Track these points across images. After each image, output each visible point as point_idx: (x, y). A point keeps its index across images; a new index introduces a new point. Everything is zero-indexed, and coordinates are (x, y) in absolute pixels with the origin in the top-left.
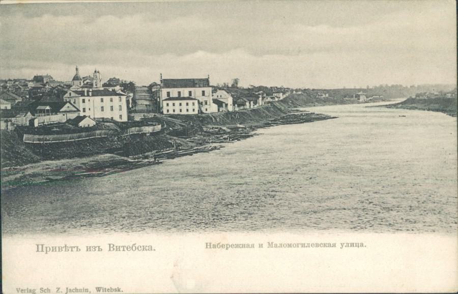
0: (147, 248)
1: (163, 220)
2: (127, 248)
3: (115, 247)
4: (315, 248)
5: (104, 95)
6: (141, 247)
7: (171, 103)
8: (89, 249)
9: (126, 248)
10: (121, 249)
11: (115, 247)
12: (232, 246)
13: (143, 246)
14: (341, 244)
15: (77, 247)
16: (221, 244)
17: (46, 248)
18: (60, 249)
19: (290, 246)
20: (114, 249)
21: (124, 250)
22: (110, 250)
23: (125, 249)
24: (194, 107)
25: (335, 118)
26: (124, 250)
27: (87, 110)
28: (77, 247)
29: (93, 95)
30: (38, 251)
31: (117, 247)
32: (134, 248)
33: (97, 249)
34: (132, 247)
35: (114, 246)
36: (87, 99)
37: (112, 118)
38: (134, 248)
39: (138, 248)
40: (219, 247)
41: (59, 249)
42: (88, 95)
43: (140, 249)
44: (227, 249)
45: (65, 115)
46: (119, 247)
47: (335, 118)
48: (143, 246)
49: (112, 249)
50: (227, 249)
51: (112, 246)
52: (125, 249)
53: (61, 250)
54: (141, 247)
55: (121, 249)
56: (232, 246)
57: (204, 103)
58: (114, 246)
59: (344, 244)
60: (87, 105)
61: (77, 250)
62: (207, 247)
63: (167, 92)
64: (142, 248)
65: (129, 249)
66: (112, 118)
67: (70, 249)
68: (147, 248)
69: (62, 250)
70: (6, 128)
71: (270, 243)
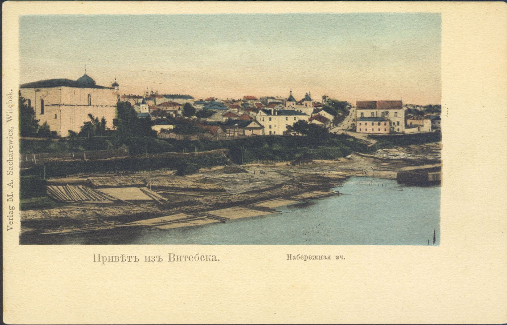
0: (211, 258)
3: (176, 257)
5: (319, 112)
6: (204, 257)
7: (363, 123)
8: (148, 259)
11: (176, 257)
12: (310, 258)
15: (342, 259)
16: (300, 256)
17: (103, 257)
18: (117, 259)
19: (315, 258)
23: (187, 259)
24: (385, 127)
27: (273, 127)
28: (342, 259)
29: (278, 114)
30: (146, 261)
32: (197, 259)
33: (133, 260)
35: (174, 255)
36: (273, 117)
38: (197, 259)
39: (309, 258)
40: (298, 258)
41: (322, 258)
42: (274, 114)
43: (203, 259)
44: (305, 260)
45: (252, 131)
49: (172, 259)
50: (305, 260)
52: (187, 259)
53: (117, 260)
54: (204, 257)
55: (183, 259)
56: (310, 258)
57: (396, 124)
58: (174, 255)
61: (159, 261)
62: (342, 256)
63: (270, 125)
64: (205, 257)
65: (191, 259)
67: (128, 260)
68: (211, 258)
69: (119, 260)
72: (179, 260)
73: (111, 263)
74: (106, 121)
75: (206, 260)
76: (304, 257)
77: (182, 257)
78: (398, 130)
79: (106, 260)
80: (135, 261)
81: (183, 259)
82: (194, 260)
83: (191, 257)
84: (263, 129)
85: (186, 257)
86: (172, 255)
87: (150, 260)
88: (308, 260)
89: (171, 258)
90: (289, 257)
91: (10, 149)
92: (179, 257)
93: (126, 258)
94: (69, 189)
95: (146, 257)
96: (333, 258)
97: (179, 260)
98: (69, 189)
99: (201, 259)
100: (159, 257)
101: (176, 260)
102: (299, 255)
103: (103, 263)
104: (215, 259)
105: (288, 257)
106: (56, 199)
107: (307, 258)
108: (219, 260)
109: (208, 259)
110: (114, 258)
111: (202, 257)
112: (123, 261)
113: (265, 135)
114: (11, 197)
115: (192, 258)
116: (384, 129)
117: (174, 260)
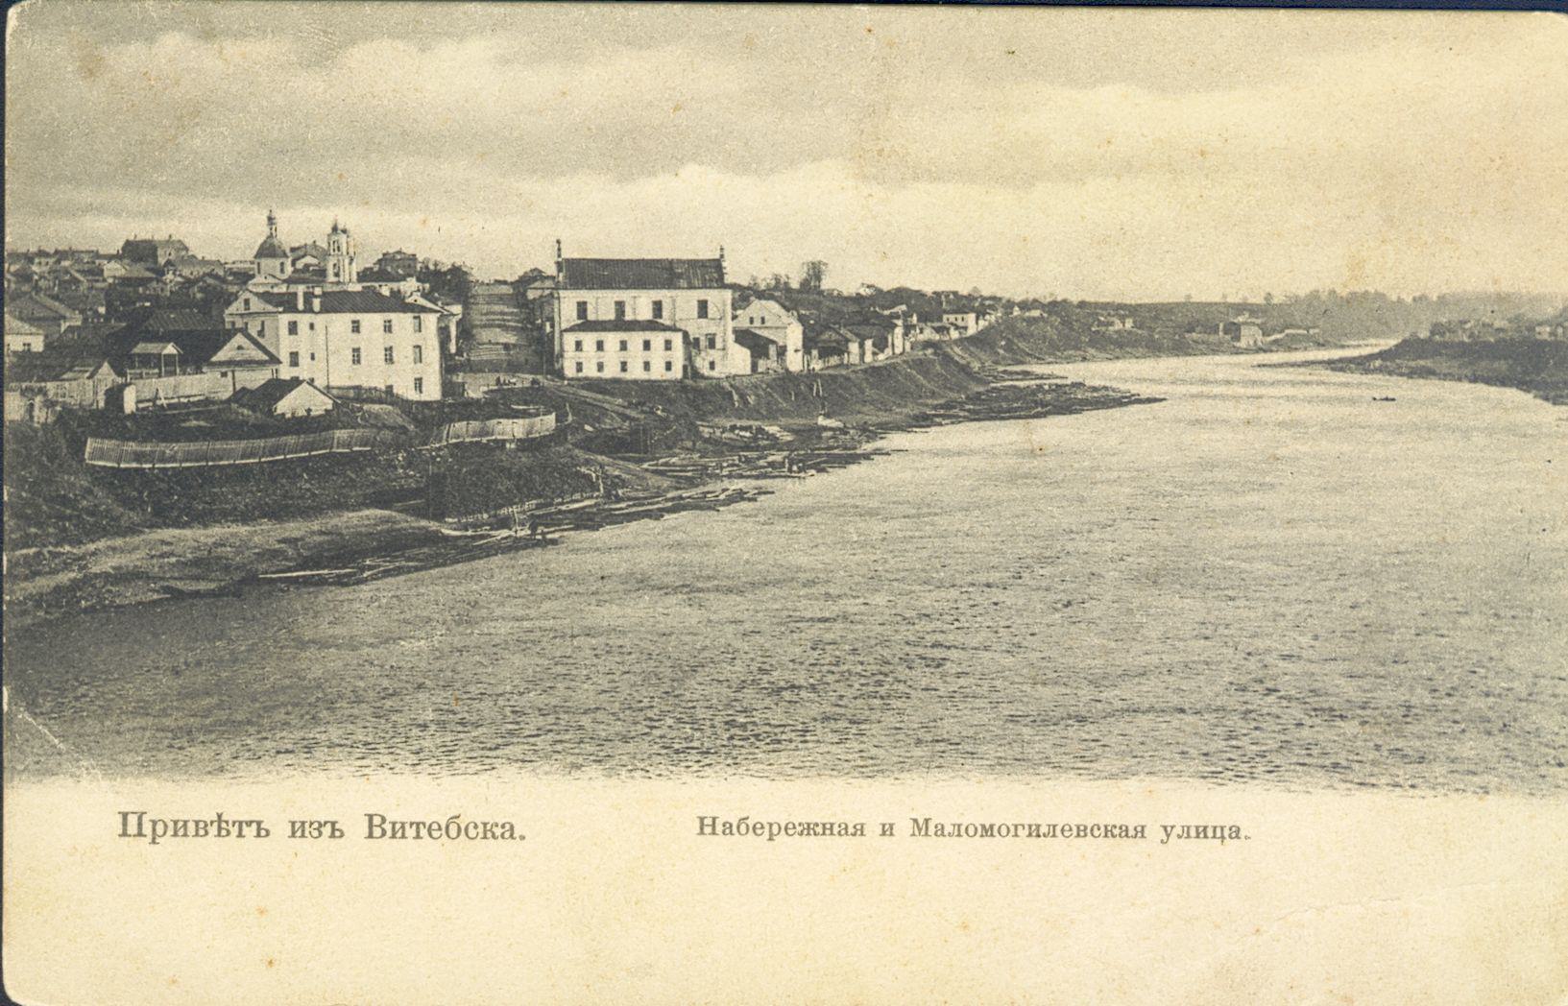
4: (1193, 844)
6: (476, 827)
7: (589, 339)
11: (388, 827)
13: (485, 824)
14: (1165, 828)
21: (418, 836)
22: (371, 836)
23: (424, 832)
25: (1156, 400)
26: (418, 836)
27: (304, 360)
29: (326, 309)
32: (453, 832)
34: (447, 827)
36: (303, 320)
38: (453, 832)
41: (1214, 831)
42: (309, 309)
43: (472, 833)
44: (771, 839)
47: (1156, 400)
48: (485, 824)
49: (377, 832)
50: (771, 839)
52: (424, 832)
55: (411, 832)
57: (703, 343)
58: (384, 820)
59: (1172, 827)
74: (132, 238)
75: (481, 835)
76: (767, 827)
77: (407, 826)
78: (712, 365)
80: (121, 832)
81: (411, 832)
82: (444, 836)
83: (435, 826)
84: (274, 368)
85: (421, 826)
86: (377, 821)
88: (782, 838)
90: (707, 826)
93: (230, 827)
96: (1155, 833)
99: (467, 835)
101: (389, 833)
102: (747, 818)
103: (154, 839)
105: (371, 826)
107: (738, 827)
108: (522, 838)
109: (489, 834)
110: (191, 826)
111: (472, 826)
113: (826, 284)
114: (923, 832)
115: (1071, 830)
116: (673, 368)
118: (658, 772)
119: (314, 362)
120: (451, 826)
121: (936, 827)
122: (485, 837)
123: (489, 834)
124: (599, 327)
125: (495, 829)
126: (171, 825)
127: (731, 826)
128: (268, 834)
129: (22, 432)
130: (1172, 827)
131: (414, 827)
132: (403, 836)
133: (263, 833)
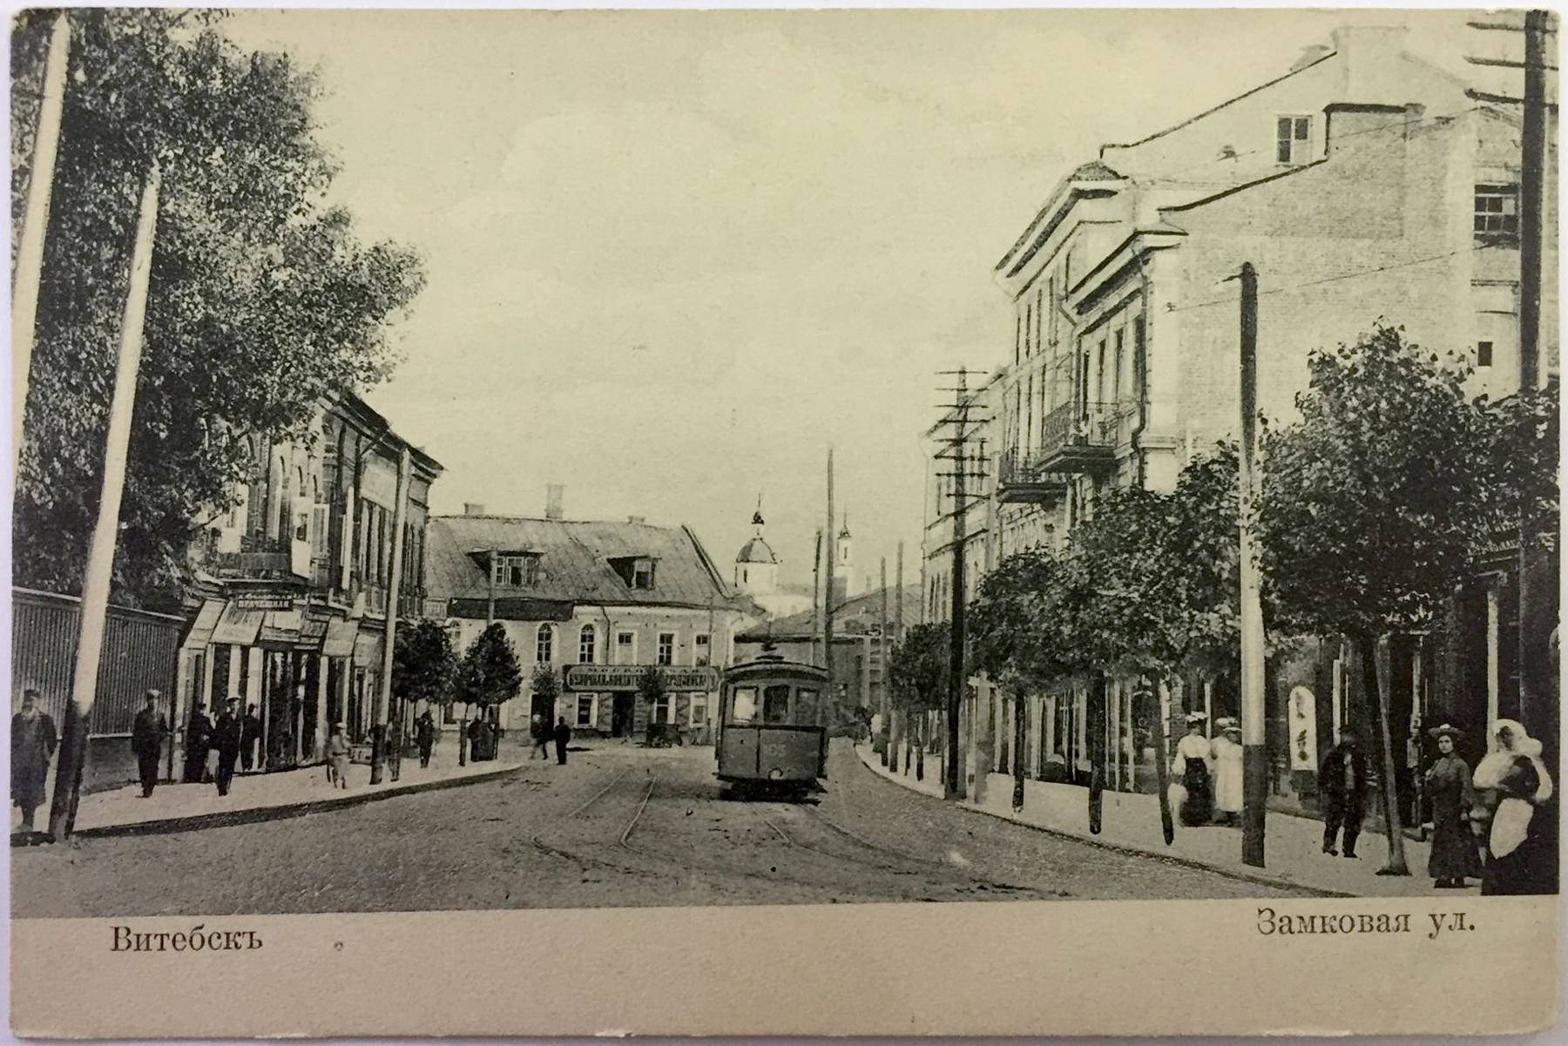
1: (717, 824)
2: (174, 941)
6: (219, 937)
9: (1308, 924)
10: (155, 943)
11: (132, 938)
13: (228, 934)
14: (466, 506)
20: (1372, 927)
31: (138, 936)
32: (197, 941)
33: (244, 941)
37: (1390, 339)
38: (197, 941)
43: (215, 943)
46: (148, 936)
49: (123, 944)
51: (1367, 919)
52: (168, 943)
54: (219, 937)
55: (155, 943)
60: (111, 252)
65: (179, 945)
66: (1390, 339)
68: (1336, 924)
70: (812, 607)
71: (1307, 919)
72: (143, 946)
73: (143, 953)
75: (224, 944)
77: (151, 938)
79: (1353, 926)
83: (179, 938)
85: (165, 938)
86: (122, 933)
87: (224, 937)
89: (120, 941)
91: (1338, 918)
92: (143, 938)
94: (1052, 458)
95: (117, 929)
97: (143, 946)
98: (1052, 458)
100: (251, 934)
101: (134, 945)
102: (201, 928)
104: (255, 943)
106: (1500, 605)
109: (232, 945)
111: (215, 936)
112: (251, 946)
114: (1309, 929)
117: (129, 946)
118: (1279, 840)
119: (932, 460)
120: (1349, 926)
121: (1281, 920)
122: (228, 947)
123: (232, 945)
124: (1485, 355)
125: (238, 939)
126: (1357, 921)
127: (1388, 918)
128: (261, 944)
129: (1320, 498)
130: (1443, 916)
131: (159, 938)
132: (148, 948)
133: (256, 944)
